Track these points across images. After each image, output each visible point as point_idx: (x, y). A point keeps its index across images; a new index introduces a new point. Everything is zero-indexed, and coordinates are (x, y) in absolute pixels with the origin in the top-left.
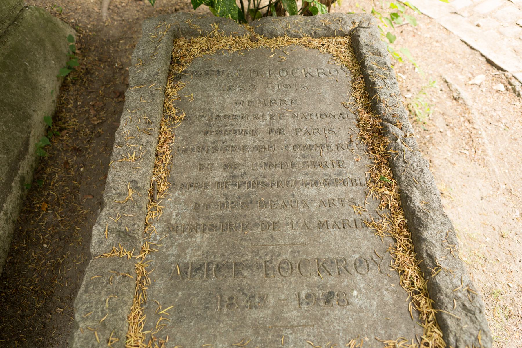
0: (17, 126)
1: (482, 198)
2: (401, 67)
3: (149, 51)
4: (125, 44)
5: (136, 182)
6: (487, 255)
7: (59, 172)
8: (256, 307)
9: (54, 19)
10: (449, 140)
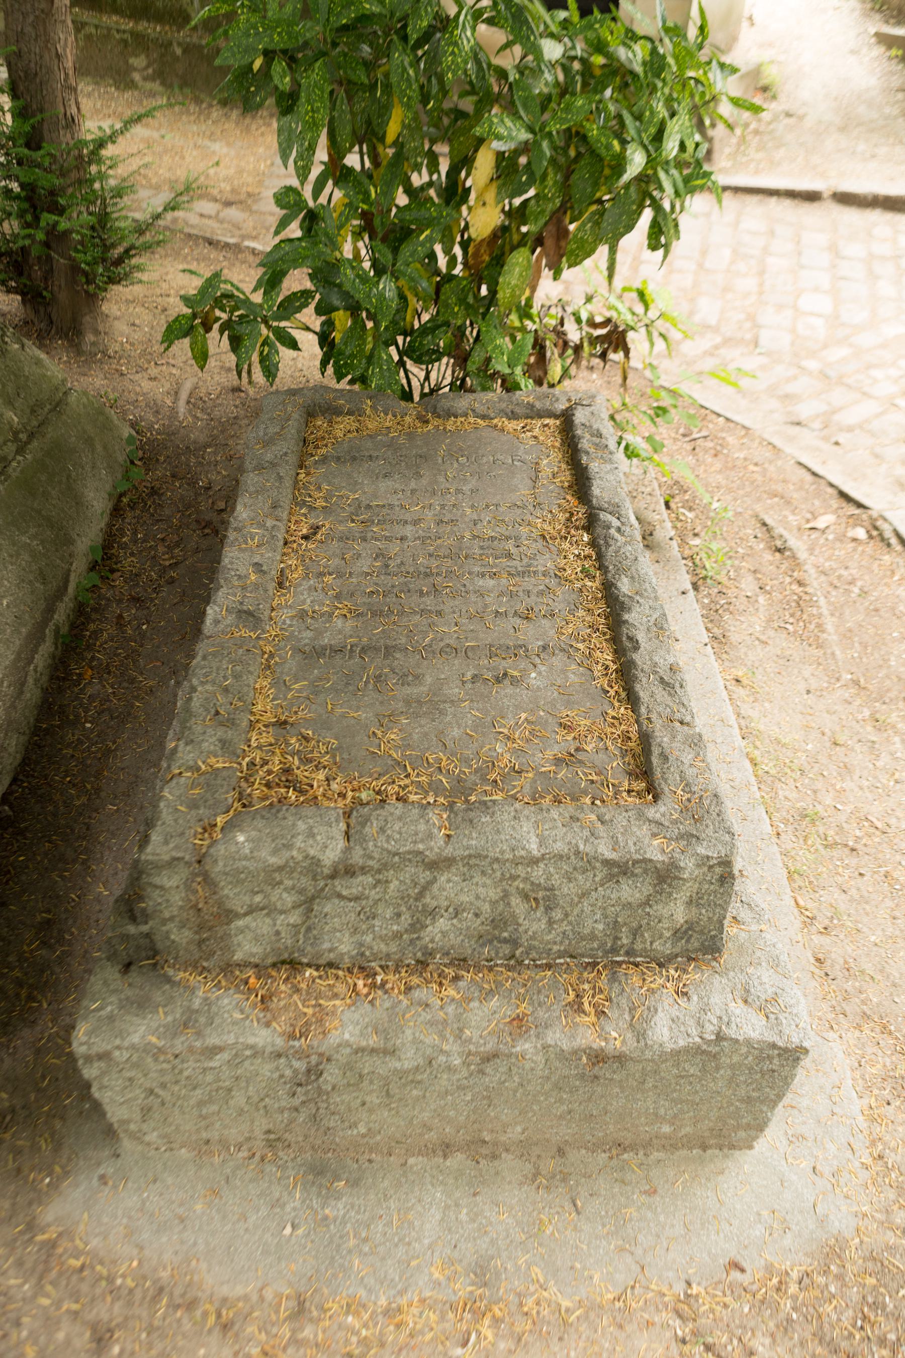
0: (57, 550)
1: (808, 692)
2: (687, 501)
3: (273, 430)
4: (215, 453)
5: (261, 566)
6: (807, 767)
7: (109, 630)
8: (409, 685)
9: (108, 410)
10: (762, 609)
